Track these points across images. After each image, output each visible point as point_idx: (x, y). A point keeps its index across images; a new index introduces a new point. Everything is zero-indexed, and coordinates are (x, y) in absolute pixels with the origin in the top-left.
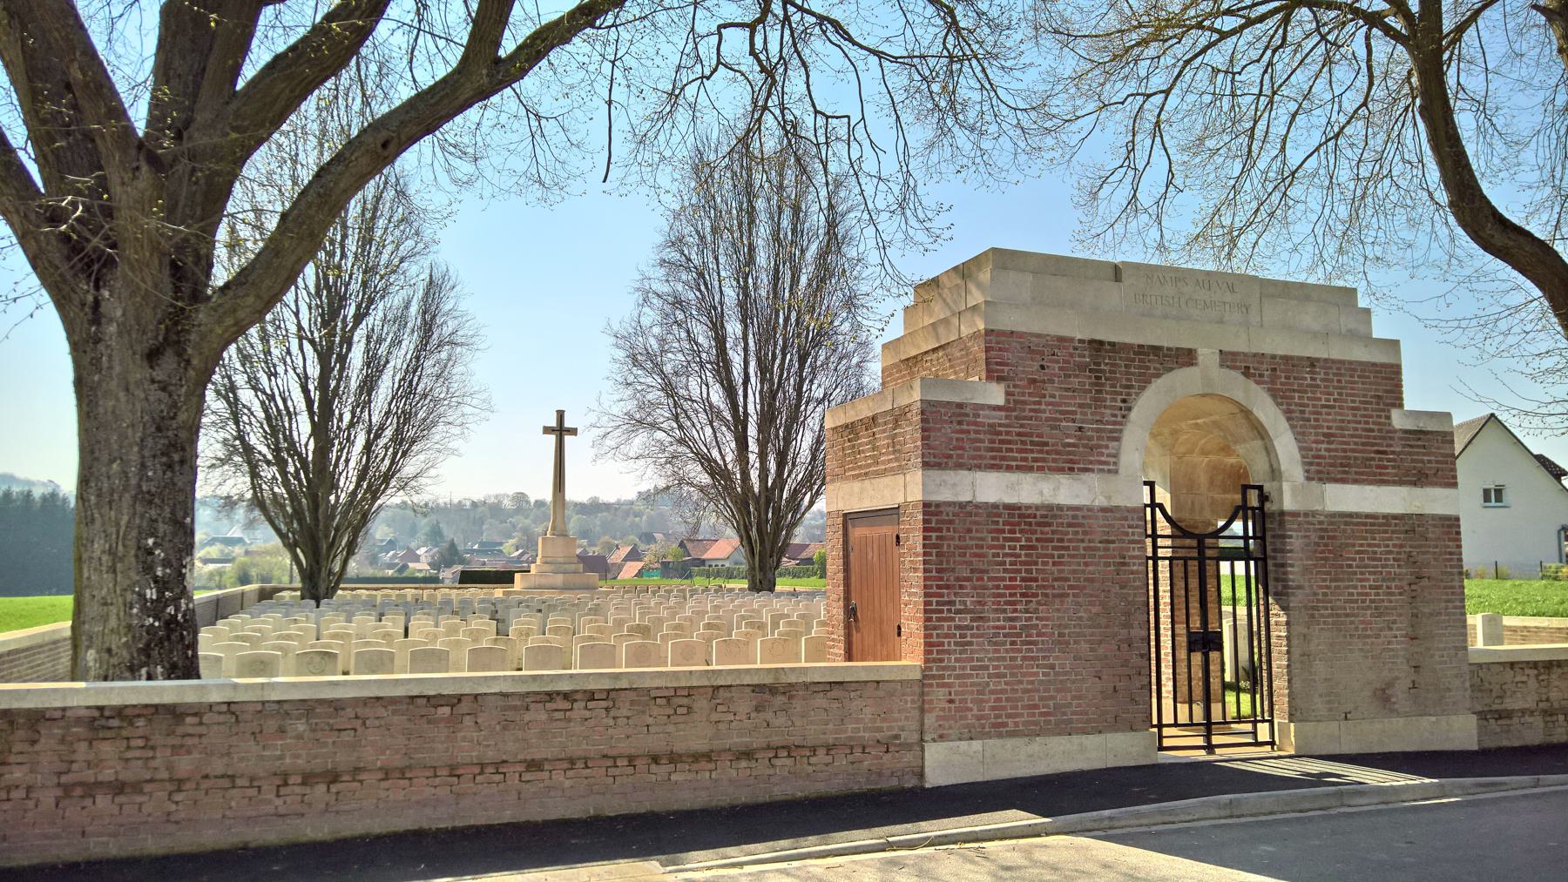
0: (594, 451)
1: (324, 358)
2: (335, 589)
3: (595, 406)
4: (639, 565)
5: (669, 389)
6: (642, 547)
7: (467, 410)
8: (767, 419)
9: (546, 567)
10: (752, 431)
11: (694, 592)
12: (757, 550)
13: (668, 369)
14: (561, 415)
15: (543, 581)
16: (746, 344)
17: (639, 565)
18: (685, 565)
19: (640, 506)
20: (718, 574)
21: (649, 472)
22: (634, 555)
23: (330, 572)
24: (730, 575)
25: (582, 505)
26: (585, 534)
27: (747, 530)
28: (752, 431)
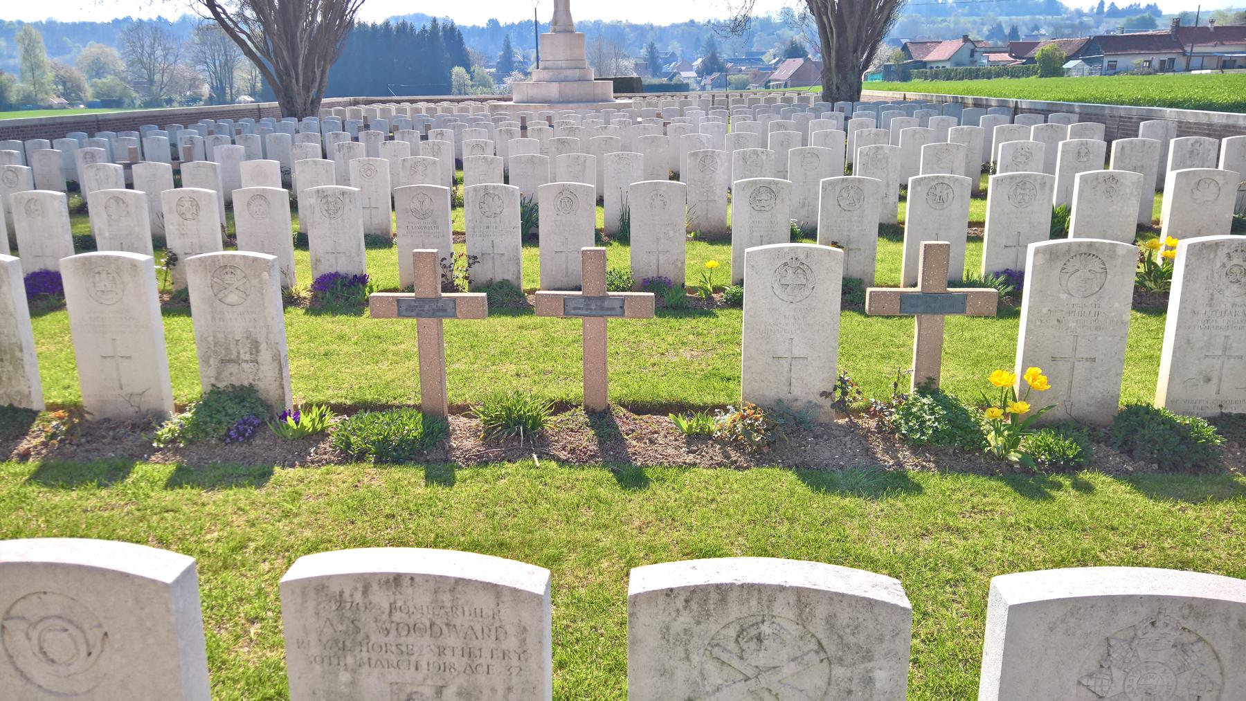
12: (834, 42)
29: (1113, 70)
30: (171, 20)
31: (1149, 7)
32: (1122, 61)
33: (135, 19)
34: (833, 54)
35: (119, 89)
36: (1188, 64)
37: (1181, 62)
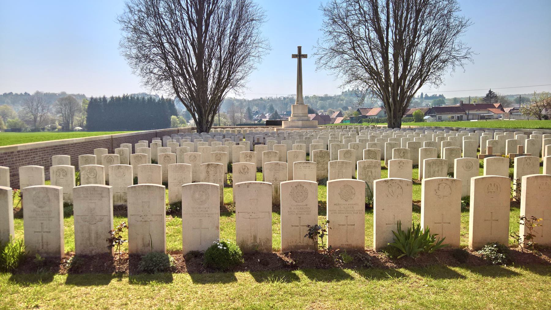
0: (316, 66)
1: (199, 30)
2: (210, 128)
3: (316, 45)
4: (342, 118)
5: (350, 34)
6: (344, 112)
7: (260, 49)
8: (398, 45)
9: (295, 118)
10: (391, 50)
11: (362, 128)
12: (392, 109)
13: (350, 25)
14: (300, 48)
15: (293, 124)
16: (388, 9)
17: (342, 118)
18: (360, 118)
19: (343, 97)
20: (373, 121)
21: (341, 74)
22: (340, 115)
23: (207, 121)
24: (378, 121)
25: (322, 97)
26: (322, 108)
27: (388, 100)
28: (391, 50)
29: (440, 119)
30: (31, 94)
31: (440, 95)
32: (444, 116)
33: (14, 93)
34: (392, 112)
35: (20, 124)
36: (468, 117)
37: (465, 117)
